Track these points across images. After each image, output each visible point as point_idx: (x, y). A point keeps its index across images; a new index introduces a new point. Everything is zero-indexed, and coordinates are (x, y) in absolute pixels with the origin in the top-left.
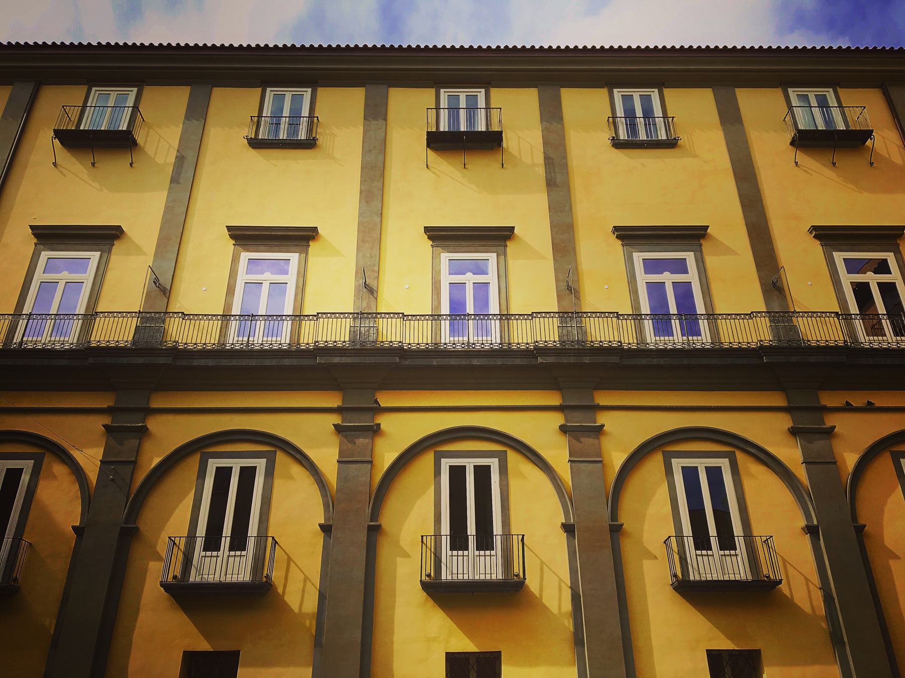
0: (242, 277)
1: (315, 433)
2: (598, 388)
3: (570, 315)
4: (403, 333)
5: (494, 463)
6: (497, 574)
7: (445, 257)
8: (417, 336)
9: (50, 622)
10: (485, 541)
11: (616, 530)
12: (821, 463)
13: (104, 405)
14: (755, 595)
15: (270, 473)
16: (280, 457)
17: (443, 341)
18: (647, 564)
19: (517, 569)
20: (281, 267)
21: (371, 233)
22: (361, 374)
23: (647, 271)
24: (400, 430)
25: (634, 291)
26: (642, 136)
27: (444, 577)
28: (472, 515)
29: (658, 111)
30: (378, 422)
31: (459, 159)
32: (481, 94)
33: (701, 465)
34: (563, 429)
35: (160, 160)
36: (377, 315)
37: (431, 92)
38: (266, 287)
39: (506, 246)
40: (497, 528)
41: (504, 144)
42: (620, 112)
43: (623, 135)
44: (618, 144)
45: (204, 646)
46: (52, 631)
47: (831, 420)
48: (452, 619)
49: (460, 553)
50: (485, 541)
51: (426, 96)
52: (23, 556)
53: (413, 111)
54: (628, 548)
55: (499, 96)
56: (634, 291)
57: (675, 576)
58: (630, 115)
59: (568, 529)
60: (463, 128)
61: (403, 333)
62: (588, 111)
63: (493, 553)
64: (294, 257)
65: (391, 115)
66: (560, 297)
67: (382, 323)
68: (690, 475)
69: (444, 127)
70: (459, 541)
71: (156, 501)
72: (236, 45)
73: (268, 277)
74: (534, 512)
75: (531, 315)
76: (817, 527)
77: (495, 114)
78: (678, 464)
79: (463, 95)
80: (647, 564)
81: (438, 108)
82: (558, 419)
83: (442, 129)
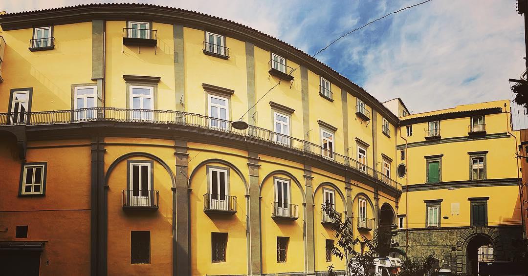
0: (132, 96)
1: (167, 155)
2: (188, 141)
3: (103, 109)
4: (167, 118)
5: (226, 172)
6: (226, 209)
7: (131, 87)
8: (121, 117)
9: (170, 221)
10: (145, 193)
11: (190, 191)
12: (182, 167)
13: (173, 145)
14: (228, 216)
15: (152, 167)
16: (155, 163)
17: (131, 119)
18: (198, 202)
19: (155, 203)
20: (146, 91)
21: (180, 83)
22: (181, 135)
23: (134, 93)
24: (196, 158)
25: (207, 108)
26: (216, 52)
27: (131, 205)
28: (218, 189)
29: (222, 45)
30: (105, 149)
31: (137, 50)
32: (148, 25)
33: (219, 171)
34: (175, 154)
35: (167, 52)
36: (185, 113)
37: (124, 23)
38: (142, 100)
39: (157, 85)
40: (226, 194)
41: (158, 45)
42: (208, 41)
43: (208, 50)
44: (205, 53)
45: (218, 231)
46: (171, 224)
47: (379, 197)
48: (278, 226)
49: (145, 197)
50: (145, 193)
51: (123, 24)
52: (294, 210)
53: (117, 30)
54: (193, 198)
55: (156, 26)
56: (207, 108)
57: (206, 207)
58: (212, 44)
59: (174, 190)
60: (139, 37)
61: (167, 118)
62: (194, 39)
63: (139, 197)
64: (152, 88)
65: (184, 38)
66: (177, 105)
67: (188, 117)
68: (215, 173)
69: (130, 36)
70: (215, 196)
71: (195, 180)
72: (131, 3)
73: (142, 96)
74: (235, 186)
75: (167, 111)
76: (249, 196)
77: (154, 33)
78: (211, 170)
79: (139, 25)
80: (198, 202)
81: (127, 28)
82: (173, 151)
83: (129, 37)
